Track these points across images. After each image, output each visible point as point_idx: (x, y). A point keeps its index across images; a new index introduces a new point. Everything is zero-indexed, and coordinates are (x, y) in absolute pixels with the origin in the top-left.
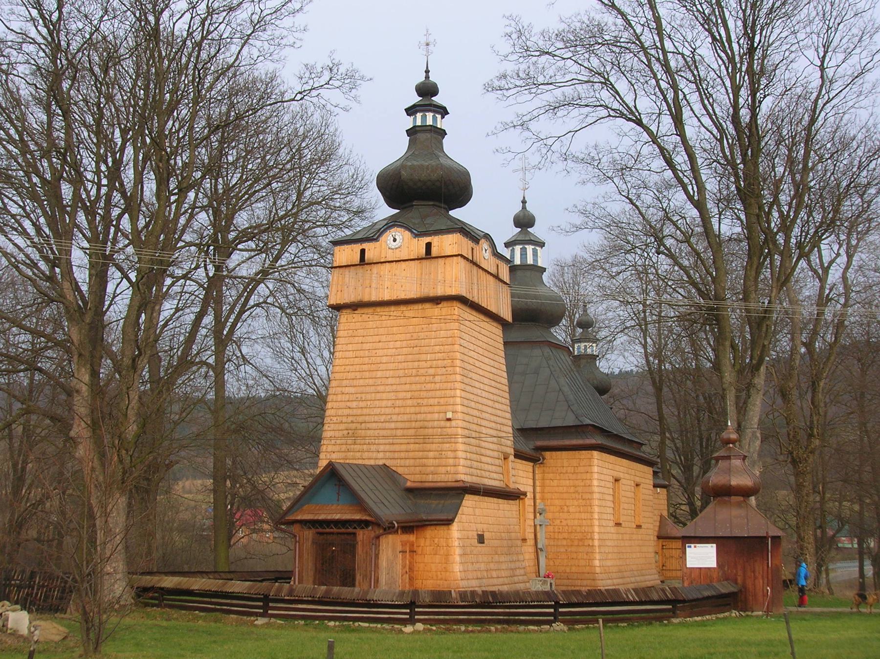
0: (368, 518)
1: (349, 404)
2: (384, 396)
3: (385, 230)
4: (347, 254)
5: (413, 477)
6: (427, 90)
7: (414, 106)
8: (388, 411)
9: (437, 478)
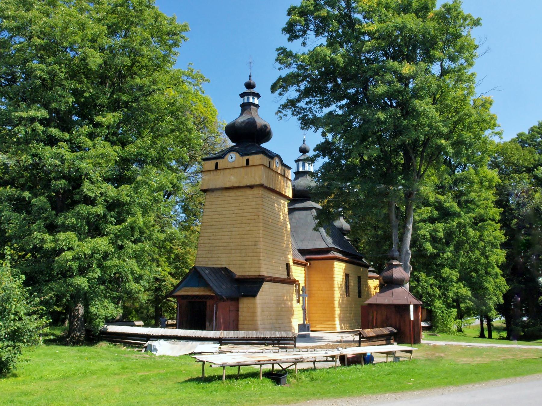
0: (208, 293)
1: (209, 238)
4: (211, 165)
5: (239, 272)
6: (249, 85)
7: (244, 93)
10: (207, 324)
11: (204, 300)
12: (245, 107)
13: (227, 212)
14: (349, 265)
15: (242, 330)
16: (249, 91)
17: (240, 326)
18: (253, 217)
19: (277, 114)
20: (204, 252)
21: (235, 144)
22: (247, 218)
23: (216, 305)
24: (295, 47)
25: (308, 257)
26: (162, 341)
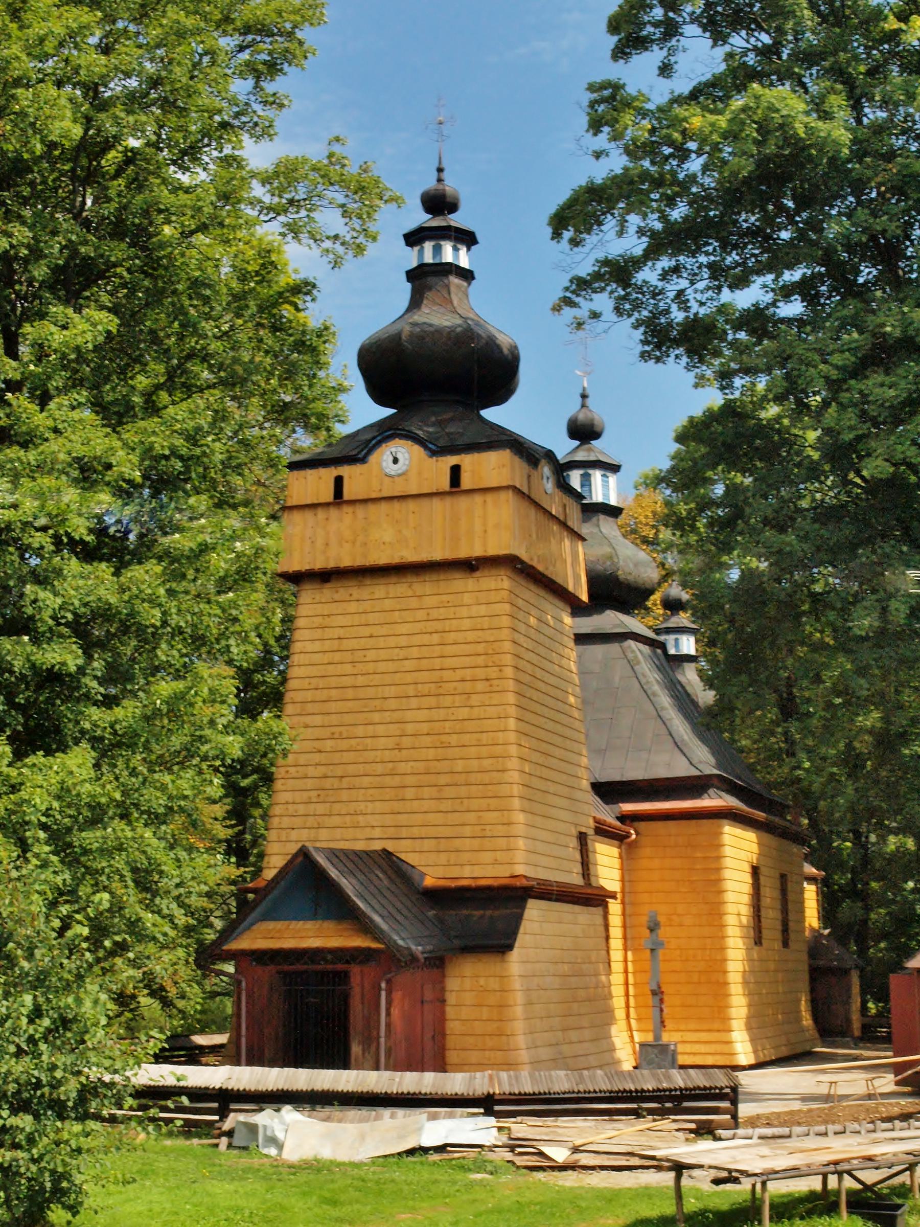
0: (374, 945)
1: (317, 744)
2: (381, 729)
3: (379, 443)
4: (316, 485)
6: (438, 203)
8: (387, 755)
9: (478, 872)
10: (356, 1049)
11: (340, 967)
12: (423, 279)
13: (383, 654)
14: (767, 837)
15: (460, 1067)
16: (438, 222)
17: (452, 1057)
18: (480, 673)
19: (557, 309)
20: (298, 796)
21: (391, 411)
22: (459, 674)
23: (389, 982)
24: (640, 75)
25: (628, 807)
26: (289, 1113)
